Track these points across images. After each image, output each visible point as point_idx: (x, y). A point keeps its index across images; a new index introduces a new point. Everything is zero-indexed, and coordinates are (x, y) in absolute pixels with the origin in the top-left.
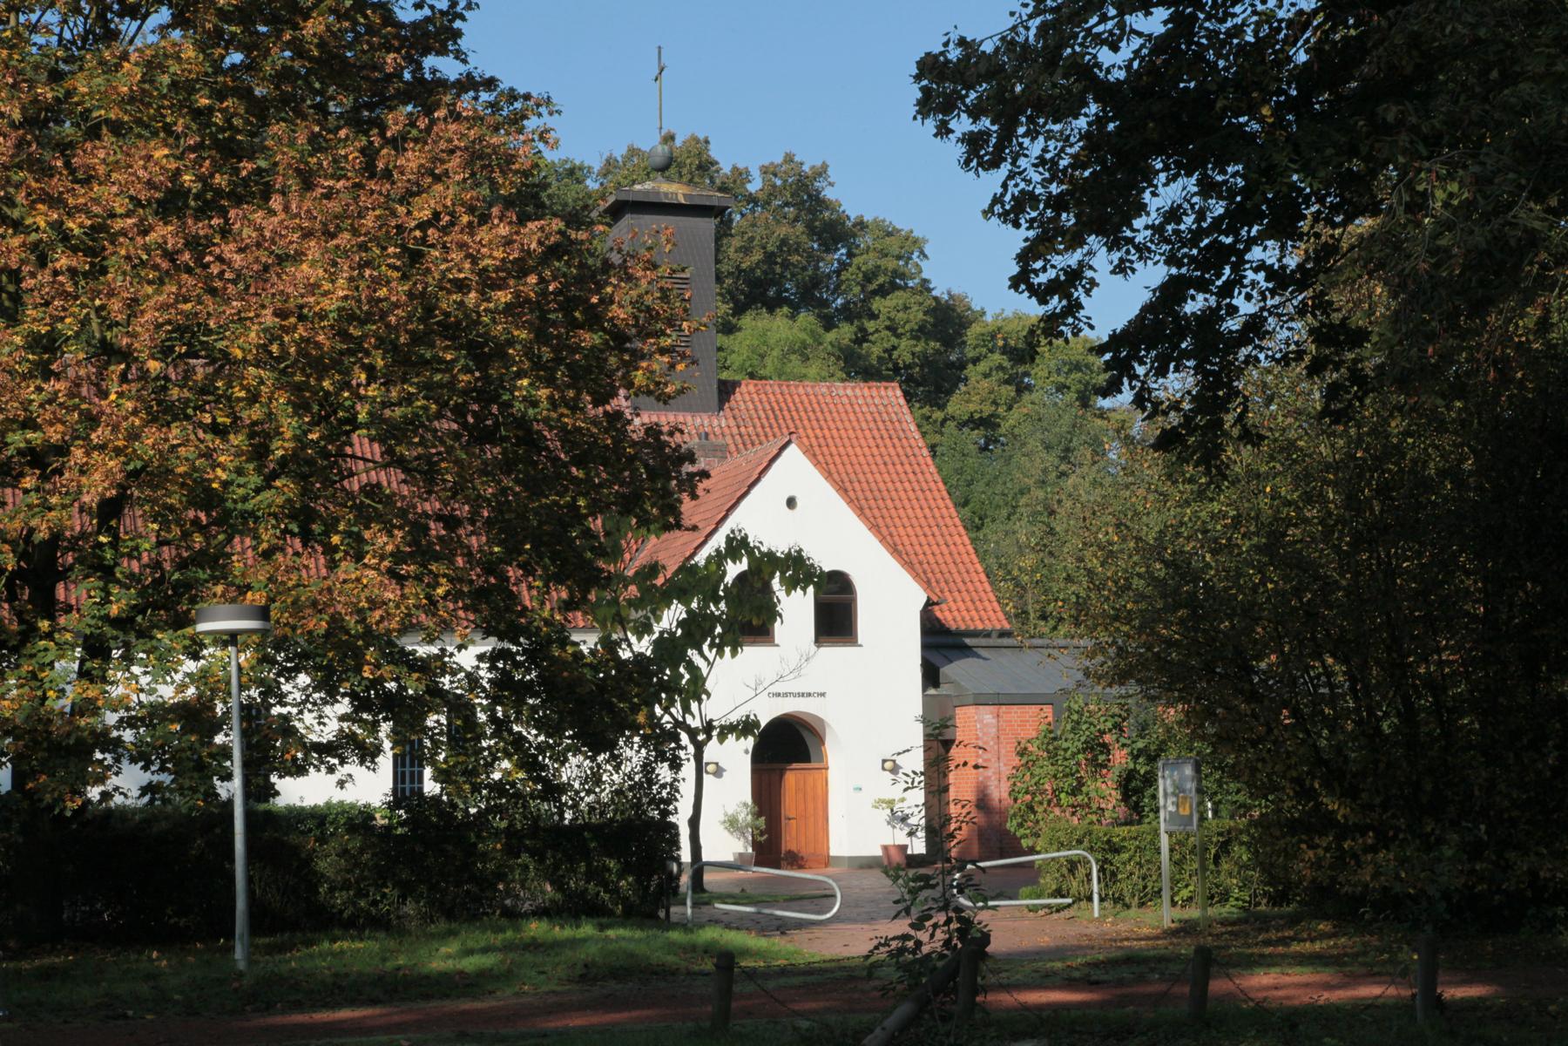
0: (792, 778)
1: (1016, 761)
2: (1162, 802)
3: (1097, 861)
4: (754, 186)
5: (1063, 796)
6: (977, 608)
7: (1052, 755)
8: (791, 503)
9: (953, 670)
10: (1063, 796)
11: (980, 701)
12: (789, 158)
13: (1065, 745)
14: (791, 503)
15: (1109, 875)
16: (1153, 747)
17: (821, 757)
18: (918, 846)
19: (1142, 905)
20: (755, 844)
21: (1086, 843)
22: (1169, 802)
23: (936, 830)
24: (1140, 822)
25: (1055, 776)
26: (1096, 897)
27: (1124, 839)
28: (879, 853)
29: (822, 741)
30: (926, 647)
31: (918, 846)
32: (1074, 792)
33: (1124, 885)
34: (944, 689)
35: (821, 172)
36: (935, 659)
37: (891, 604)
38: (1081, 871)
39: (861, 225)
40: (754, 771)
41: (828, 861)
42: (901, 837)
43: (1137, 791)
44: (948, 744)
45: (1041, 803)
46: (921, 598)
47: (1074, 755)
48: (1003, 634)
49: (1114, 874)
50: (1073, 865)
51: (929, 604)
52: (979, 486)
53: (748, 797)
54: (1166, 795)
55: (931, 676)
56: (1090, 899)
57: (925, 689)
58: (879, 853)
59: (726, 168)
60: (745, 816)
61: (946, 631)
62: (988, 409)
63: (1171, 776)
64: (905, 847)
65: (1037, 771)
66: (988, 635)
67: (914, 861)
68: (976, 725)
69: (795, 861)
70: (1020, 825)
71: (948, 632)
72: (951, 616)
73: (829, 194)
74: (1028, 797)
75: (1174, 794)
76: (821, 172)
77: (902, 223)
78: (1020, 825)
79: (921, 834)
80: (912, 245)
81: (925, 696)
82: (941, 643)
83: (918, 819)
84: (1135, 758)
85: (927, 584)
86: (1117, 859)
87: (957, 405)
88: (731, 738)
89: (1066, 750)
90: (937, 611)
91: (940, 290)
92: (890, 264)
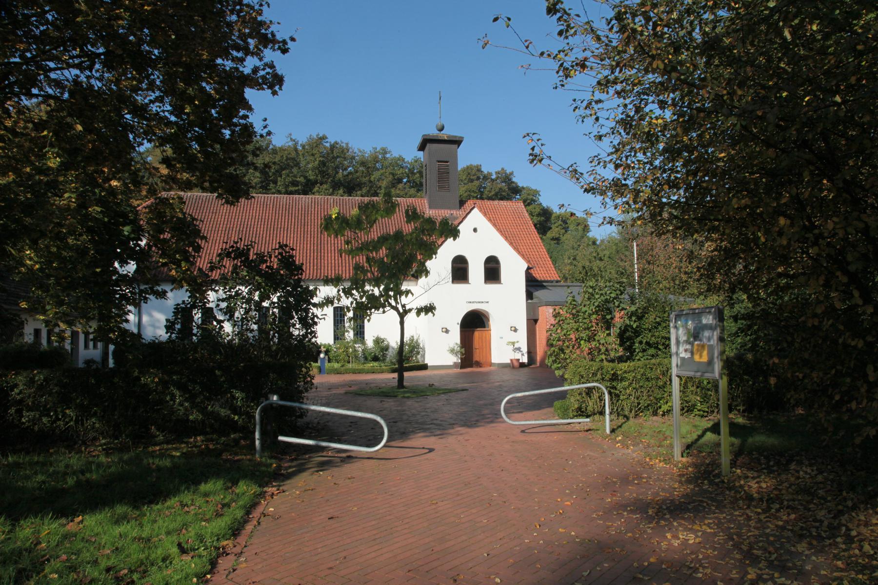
0: (477, 334)
1: (553, 321)
2: (673, 348)
3: (607, 387)
4: (494, 177)
5: (582, 342)
6: (546, 272)
7: (575, 316)
8: (475, 230)
9: (539, 294)
10: (582, 342)
11: (548, 304)
12: (503, 169)
13: (584, 309)
14: (475, 230)
15: (615, 396)
16: (640, 311)
17: (489, 326)
18: (525, 360)
19: (636, 416)
20: (461, 359)
21: (599, 376)
22: (681, 349)
23: (531, 353)
24: (629, 358)
25: (577, 329)
26: (607, 411)
27: (625, 372)
28: (509, 362)
29: (488, 320)
30: (527, 286)
31: (525, 360)
32: (590, 339)
33: (624, 403)
34: (535, 300)
35: (512, 173)
36: (531, 289)
37: (514, 268)
38: (596, 395)
39: (523, 188)
40: (461, 331)
41: (491, 364)
42: (518, 356)
43: (629, 338)
44: (536, 321)
45: (568, 347)
46: (525, 266)
47: (590, 315)
48: (557, 282)
49: (618, 396)
50: (589, 391)
51: (529, 269)
52: (555, 253)
53: (459, 342)
54: (678, 343)
55: (529, 295)
56: (602, 413)
57: (527, 300)
58: (509, 362)
59: (486, 172)
60: (457, 348)
61: (536, 280)
62: (557, 236)
63: (685, 326)
64: (518, 360)
65: (565, 326)
66: (552, 282)
67: (522, 365)
68: (546, 314)
69: (478, 364)
70: (554, 362)
71: (537, 281)
72: (539, 275)
73: (514, 180)
74: (560, 343)
75: (687, 342)
76: (512, 173)
77: (534, 187)
78: (554, 362)
79: (526, 355)
80: (536, 193)
81: (527, 303)
82: (533, 284)
83: (525, 349)
84: (630, 318)
85: (528, 262)
86: (620, 386)
87: (550, 235)
88: (423, 314)
89: (585, 313)
90: (532, 271)
91: (545, 205)
92: (530, 197)
